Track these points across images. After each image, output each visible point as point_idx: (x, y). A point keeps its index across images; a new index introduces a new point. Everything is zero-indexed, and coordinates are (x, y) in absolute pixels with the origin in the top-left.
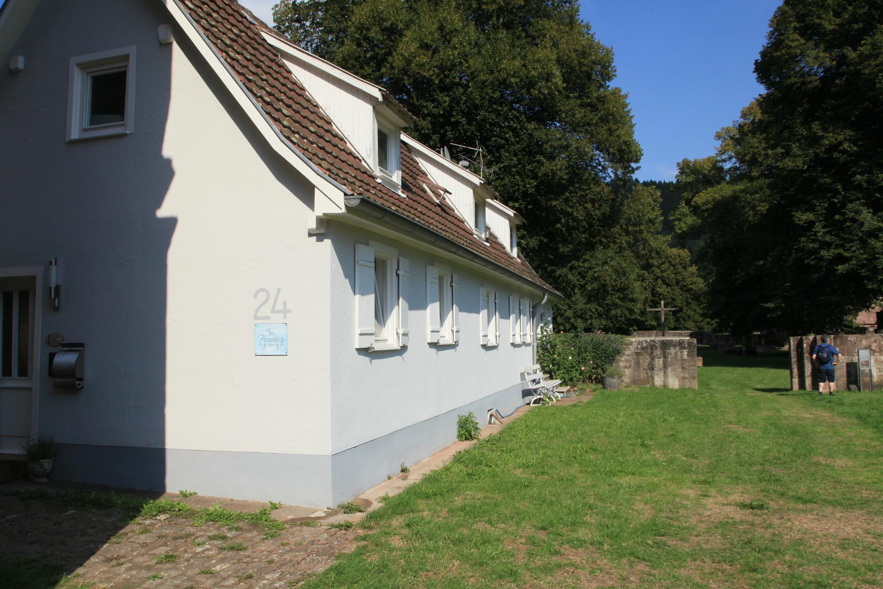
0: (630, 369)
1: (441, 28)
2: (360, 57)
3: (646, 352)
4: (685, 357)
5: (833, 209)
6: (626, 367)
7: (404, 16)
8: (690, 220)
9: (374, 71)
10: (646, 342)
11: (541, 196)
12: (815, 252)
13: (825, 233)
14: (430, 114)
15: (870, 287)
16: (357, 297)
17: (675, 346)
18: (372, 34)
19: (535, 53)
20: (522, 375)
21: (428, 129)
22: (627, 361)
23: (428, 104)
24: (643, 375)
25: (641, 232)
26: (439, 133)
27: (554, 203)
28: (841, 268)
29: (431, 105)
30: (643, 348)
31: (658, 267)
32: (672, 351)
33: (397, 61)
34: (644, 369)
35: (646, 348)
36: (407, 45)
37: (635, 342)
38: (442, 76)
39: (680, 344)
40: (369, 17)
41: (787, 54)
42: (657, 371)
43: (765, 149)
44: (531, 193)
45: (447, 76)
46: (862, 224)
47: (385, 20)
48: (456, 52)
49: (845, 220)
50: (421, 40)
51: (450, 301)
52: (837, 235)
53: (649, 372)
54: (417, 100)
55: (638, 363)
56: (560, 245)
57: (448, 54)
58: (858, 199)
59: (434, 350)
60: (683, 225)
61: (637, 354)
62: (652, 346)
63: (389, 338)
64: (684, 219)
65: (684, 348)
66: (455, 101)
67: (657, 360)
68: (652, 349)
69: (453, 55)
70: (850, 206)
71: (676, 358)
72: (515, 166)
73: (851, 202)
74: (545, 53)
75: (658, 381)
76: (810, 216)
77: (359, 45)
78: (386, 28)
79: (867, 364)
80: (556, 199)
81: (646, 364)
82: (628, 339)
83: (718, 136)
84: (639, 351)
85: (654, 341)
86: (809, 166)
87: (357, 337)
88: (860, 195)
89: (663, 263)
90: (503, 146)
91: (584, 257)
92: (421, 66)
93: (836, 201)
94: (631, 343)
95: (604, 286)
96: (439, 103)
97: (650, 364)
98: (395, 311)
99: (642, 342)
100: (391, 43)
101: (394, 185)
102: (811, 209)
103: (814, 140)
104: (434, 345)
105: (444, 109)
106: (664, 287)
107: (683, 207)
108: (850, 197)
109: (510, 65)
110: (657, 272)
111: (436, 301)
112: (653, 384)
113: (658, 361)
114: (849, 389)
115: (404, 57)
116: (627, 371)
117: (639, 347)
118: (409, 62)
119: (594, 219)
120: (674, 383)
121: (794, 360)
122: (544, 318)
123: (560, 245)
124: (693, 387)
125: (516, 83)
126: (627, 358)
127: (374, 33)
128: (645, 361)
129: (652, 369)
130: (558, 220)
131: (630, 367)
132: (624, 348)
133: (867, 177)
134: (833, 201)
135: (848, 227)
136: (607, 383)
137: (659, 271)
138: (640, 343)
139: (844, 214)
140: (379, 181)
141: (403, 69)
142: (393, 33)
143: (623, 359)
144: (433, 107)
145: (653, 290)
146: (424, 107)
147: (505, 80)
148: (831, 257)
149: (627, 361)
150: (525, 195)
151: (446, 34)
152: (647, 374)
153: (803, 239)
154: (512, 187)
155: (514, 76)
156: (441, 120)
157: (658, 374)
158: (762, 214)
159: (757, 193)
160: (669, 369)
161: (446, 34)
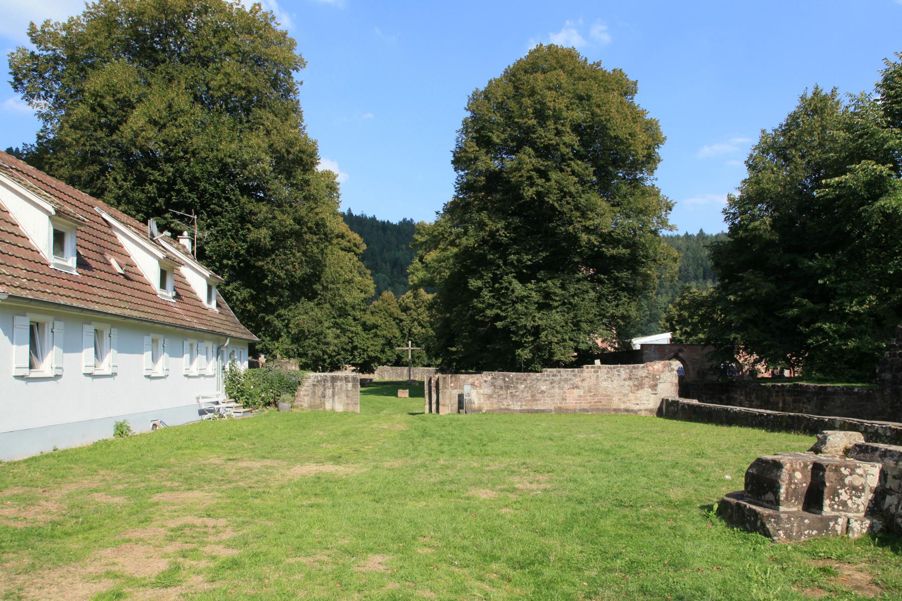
1: (170, 106)
2: (94, 121)
4: (349, 389)
5: (496, 279)
6: (305, 396)
7: (136, 91)
8: (421, 274)
9: (107, 136)
10: (321, 376)
11: (251, 256)
12: (483, 311)
13: (491, 297)
14: (155, 181)
15: (513, 339)
16: (15, 346)
17: (341, 380)
18: (105, 102)
19: (250, 139)
20: (198, 398)
21: (154, 193)
22: (306, 390)
23: (154, 172)
24: (318, 401)
25: (338, 289)
26: (164, 197)
27: (260, 263)
28: (499, 324)
29: (157, 173)
30: (318, 381)
31: (416, 311)
32: (339, 383)
33: (126, 130)
35: (321, 381)
36: (137, 119)
38: (167, 150)
39: (346, 379)
40: (104, 86)
41: (465, 157)
43: (450, 227)
44: (242, 254)
45: (172, 151)
46: (513, 291)
47: (118, 93)
48: (181, 131)
49: (502, 288)
50: (150, 116)
51: (109, 347)
52: (498, 299)
53: (322, 399)
54: (145, 168)
55: (314, 392)
56: (268, 297)
57: (172, 132)
58: (511, 273)
59: (149, 380)
60: (415, 278)
61: (314, 385)
62: (325, 380)
63: (159, 370)
64: (416, 273)
65: (349, 382)
66: (179, 172)
69: (178, 133)
70: (505, 277)
71: (341, 389)
72: (229, 230)
73: (507, 274)
74: (256, 140)
75: (328, 406)
76: (479, 283)
77: (93, 109)
78: (118, 100)
79: (469, 395)
80: (263, 260)
81: (320, 393)
83: (665, 139)
85: (326, 376)
86: (479, 245)
87: (14, 369)
88: (513, 270)
89: (420, 307)
90: (220, 214)
92: (149, 139)
93: (498, 273)
94: (310, 377)
96: (164, 172)
97: (323, 393)
98: (50, 354)
100: (124, 114)
101: (70, 268)
102: (481, 277)
103: (481, 225)
104: (148, 377)
105: (169, 178)
106: (419, 328)
109: (228, 147)
110: (414, 314)
111: (89, 347)
114: (459, 412)
115: (133, 130)
118: (136, 135)
119: (296, 278)
120: (339, 408)
121: (426, 392)
122: (232, 356)
123: (268, 297)
124: (356, 411)
125: (232, 163)
127: (107, 101)
128: (319, 391)
129: (324, 397)
130: (266, 277)
131: (308, 395)
136: (280, 406)
137: (416, 314)
138: (316, 377)
140: (52, 267)
141: (132, 140)
142: (127, 105)
143: (303, 389)
144: (159, 175)
145: (410, 330)
146: (151, 174)
147: (222, 159)
149: (306, 390)
150: (237, 255)
151: (173, 113)
153: (475, 300)
154: (226, 248)
155: (230, 157)
156: (166, 186)
158: (446, 279)
159: (444, 261)
160: (336, 397)
161: (173, 113)
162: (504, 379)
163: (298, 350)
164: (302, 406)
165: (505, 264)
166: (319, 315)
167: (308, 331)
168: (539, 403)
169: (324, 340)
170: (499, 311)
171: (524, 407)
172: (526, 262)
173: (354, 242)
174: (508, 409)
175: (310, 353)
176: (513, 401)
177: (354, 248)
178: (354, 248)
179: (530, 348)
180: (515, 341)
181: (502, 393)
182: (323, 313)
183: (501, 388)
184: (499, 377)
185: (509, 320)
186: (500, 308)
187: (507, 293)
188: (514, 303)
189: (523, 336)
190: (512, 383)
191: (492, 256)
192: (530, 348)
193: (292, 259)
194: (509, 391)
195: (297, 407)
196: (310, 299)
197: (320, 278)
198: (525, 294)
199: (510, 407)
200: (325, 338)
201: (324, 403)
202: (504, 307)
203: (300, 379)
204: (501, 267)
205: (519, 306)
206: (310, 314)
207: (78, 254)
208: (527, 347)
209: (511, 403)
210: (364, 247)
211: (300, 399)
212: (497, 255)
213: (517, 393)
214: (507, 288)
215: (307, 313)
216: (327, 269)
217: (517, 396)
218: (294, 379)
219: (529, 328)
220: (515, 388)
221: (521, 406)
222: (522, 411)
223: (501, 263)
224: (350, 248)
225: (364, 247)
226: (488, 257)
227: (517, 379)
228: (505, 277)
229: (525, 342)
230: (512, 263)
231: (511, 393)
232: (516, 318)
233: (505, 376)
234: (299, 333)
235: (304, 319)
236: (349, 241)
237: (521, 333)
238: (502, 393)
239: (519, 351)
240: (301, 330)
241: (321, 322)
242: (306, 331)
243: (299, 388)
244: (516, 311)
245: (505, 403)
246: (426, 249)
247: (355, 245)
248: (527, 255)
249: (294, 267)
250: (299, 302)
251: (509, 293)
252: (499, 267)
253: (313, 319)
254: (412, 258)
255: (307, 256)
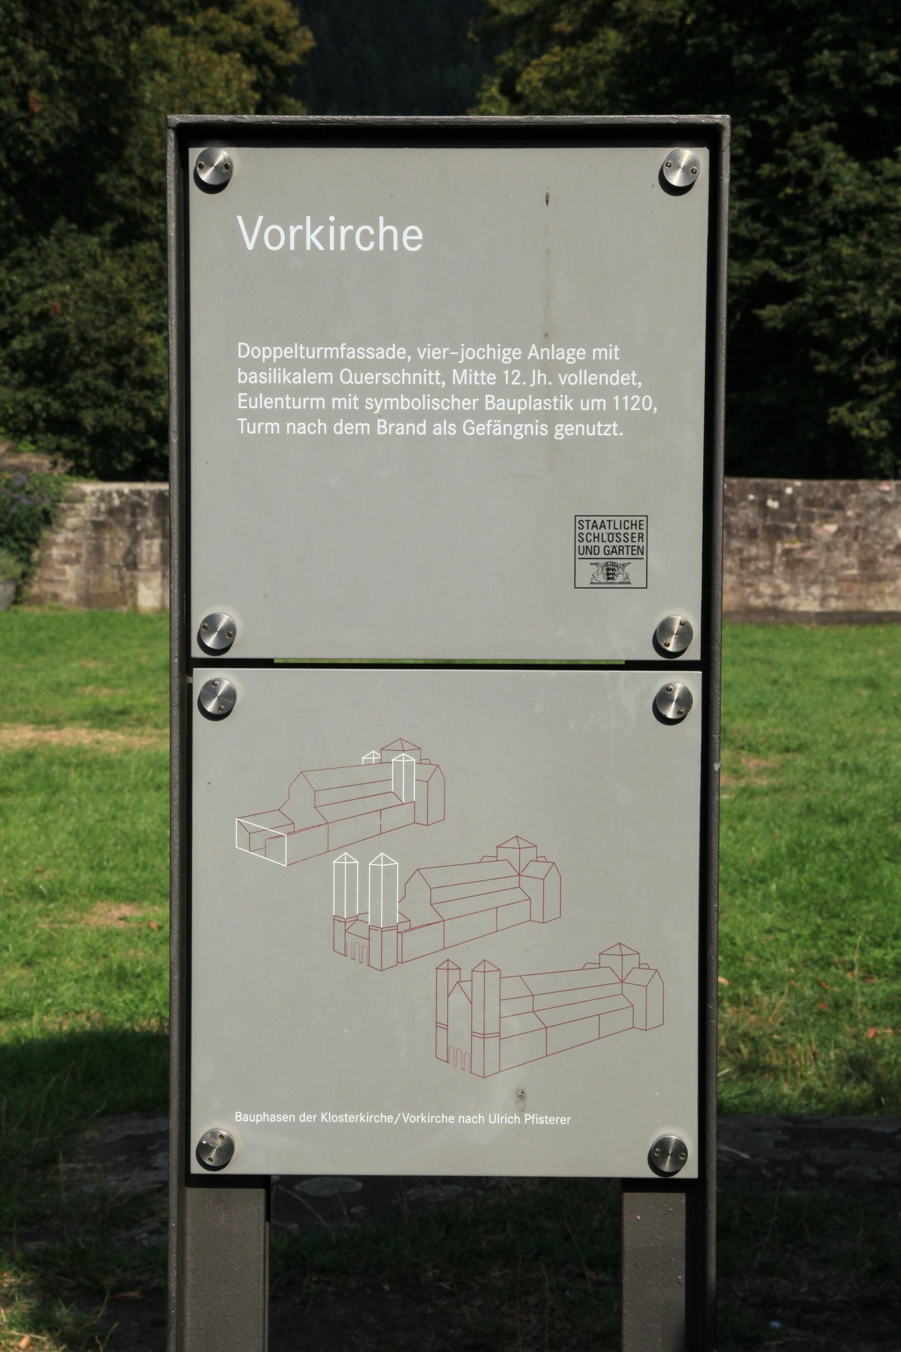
0: (77, 567)
3: (120, 523)
6: (66, 561)
10: (120, 494)
15: (820, 368)
24: (111, 582)
30: (111, 512)
34: (113, 566)
35: (121, 510)
37: (93, 493)
42: (144, 570)
46: (826, 189)
49: (785, 180)
52: (771, 222)
55: (98, 551)
58: (821, 118)
61: (98, 526)
62: (135, 507)
67: (145, 542)
68: (134, 514)
70: (798, 138)
73: (804, 126)
81: (119, 554)
82: (75, 485)
84: (101, 518)
85: (138, 493)
88: (827, 109)
91: (14, 254)
93: (772, 121)
94: (82, 498)
95: (58, 341)
99: (110, 494)
107: (492, 99)
108: (804, 111)
112: (135, 606)
113: (149, 546)
116: (71, 572)
117: (103, 507)
119: (30, 144)
126: (71, 536)
131: (76, 561)
132: (64, 510)
133: (844, 58)
134: (765, 123)
135: (790, 199)
138: (104, 497)
139: (782, 162)
143: (60, 539)
148: (748, 283)
149: (69, 544)
152: (121, 579)
157: (147, 580)
162: (762, 504)
163: (47, 406)
164: (55, 597)
165: (798, 87)
166: (119, 281)
167: (83, 339)
168: (888, 588)
169: (136, 373)
170: (771, 266)
171: (834, 604)
172: (876, 75)
173: (268, 20)
174: (775, 612)
175: (88, 418)
176: (793, 581)
177: (270, 47)
178: (270, 47)
179: (883, 399)
180: (827, 375)
181: (753, 551)
182: (133, 276)
183: (752, 535)
184: (743, 495)
185: (809, 298)
186: (776, 254)
187: (803, 198)
188: (828, 231)
189: (856, 356)
190: (792, 518)
191: (748, 58)
192: (883, 399)
193: (17, 76)
194: (779, 548)
195: (38, 600)
196: (88, 226)
197: (119, 145)
198: (871, 198)
199: (781, 604)
200: (141, 363)
201: (133, 589)
202: (790, 252)
203: (47, 504)
204: (784, 99)
205: (843, 247)
206: (87, 276)
207: (102, 1114)
208: (871, 398)
209: (786, 588)
210: (305, 40)
211: (48, 574)
212: (772, 55)
213: (809, 555)
214: (802, 179)
215: (75, 274)
216: (146, 114)
217: (809, 565)
218: (25, 502)
219: (880, 325)
220: (804, 534)
221: (824, 599)
222: (826, 618)
223: (783, 83)
224: (252, 45)
225: (305, 40)
226: (736, 62)
227: (810, 503)
228: (798, 138)
229: (866, 378)
230: (825, 82)
231: (787, 552)
232: (834, 291)
233: (764, 493)
234: (50, 346)
235: (64, 295)
236: (249, 20)
237: (849, 343)
238: (753, 551)
239: (843, 411)
240: (57, 336)
241: (124, 308)
242: (73, 336)
243: (46, 534)
244: (835, 265)
245: (766, 589)
246: (527, 45)
247: (271, 33)
248: (881, 46)
249: (24, 105)
250: (47, 235)
251: (814, 197)
252: (775, 98)
253: (98, 297)
254: (476, 83)
255: (66, 65)
